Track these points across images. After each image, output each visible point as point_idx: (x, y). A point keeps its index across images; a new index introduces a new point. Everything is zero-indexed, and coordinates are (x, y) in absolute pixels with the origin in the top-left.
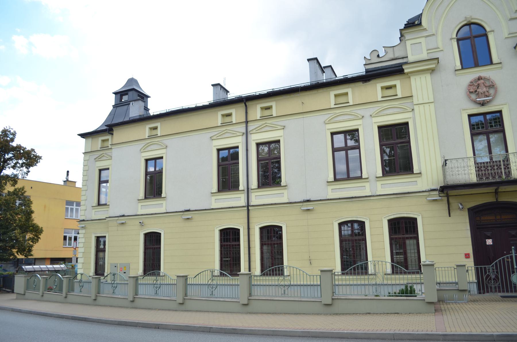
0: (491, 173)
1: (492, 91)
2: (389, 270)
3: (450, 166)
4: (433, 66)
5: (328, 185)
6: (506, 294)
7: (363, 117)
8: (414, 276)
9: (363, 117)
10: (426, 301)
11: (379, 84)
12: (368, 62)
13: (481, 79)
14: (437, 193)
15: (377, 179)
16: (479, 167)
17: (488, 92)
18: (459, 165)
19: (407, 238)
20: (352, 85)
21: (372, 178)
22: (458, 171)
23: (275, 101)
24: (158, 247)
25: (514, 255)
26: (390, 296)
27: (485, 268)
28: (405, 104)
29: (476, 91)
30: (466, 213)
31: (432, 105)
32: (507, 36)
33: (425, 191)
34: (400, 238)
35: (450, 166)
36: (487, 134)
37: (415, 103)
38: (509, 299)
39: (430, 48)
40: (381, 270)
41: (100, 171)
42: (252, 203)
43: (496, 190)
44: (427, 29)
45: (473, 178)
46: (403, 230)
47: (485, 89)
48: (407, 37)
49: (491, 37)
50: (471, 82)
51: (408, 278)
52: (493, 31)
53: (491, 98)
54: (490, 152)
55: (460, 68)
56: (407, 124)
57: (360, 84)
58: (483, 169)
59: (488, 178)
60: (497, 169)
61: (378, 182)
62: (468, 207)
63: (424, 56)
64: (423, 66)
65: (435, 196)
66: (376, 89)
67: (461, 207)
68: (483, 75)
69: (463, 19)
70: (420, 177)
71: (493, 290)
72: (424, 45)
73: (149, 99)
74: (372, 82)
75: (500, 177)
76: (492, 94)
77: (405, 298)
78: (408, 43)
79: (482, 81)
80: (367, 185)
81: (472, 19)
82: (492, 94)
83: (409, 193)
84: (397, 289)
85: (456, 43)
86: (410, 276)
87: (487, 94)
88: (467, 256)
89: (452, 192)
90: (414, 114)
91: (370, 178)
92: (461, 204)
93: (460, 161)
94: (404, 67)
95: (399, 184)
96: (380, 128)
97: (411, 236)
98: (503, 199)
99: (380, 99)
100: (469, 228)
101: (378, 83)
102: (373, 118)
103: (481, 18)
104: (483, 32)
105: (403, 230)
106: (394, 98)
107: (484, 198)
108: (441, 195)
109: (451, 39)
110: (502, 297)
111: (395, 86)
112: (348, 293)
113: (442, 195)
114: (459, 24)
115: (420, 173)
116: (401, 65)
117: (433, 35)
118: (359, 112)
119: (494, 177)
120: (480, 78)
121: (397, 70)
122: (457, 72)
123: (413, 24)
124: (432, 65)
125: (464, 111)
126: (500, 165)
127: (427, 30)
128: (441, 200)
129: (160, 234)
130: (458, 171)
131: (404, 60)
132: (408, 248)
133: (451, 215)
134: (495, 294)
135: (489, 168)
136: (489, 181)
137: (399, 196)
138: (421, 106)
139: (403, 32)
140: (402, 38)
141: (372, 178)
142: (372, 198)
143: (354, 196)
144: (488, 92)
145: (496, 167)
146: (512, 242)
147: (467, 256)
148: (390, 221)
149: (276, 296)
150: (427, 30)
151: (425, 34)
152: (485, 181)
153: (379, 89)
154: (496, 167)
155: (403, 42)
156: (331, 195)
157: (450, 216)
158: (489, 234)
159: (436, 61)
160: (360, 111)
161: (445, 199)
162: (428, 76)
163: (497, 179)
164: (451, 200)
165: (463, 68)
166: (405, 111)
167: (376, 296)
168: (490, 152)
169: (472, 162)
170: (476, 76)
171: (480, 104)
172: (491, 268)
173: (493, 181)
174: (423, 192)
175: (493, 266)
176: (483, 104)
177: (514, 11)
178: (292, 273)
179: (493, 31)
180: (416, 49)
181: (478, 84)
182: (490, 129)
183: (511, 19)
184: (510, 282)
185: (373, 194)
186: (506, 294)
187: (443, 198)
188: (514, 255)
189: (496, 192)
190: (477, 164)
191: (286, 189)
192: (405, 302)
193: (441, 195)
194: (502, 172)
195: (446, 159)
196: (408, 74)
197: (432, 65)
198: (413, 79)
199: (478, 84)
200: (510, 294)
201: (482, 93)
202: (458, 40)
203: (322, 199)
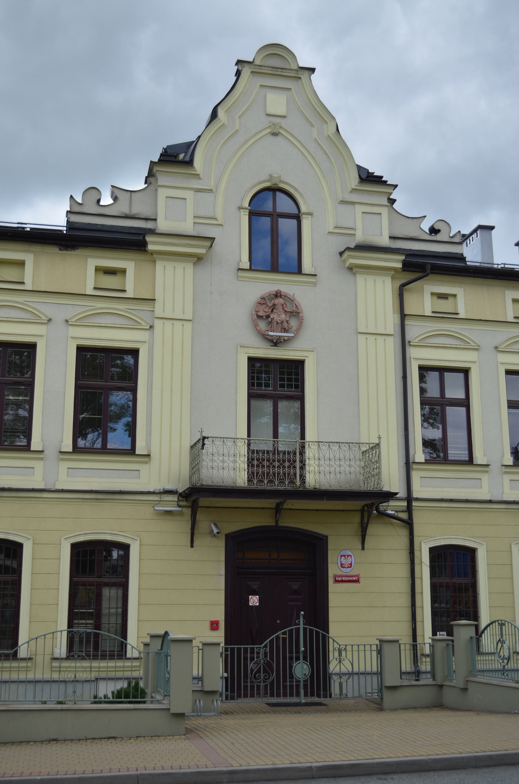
0: (279, 474)
1: (294, 323)
2: (62, 650)
3: (210, 451)
4: (202, 251)
5: (62, 460)
6: (275, 700)
7: (50, 320)
8: (111, 664)
9: (50, 320)
10: (173, 711)
11: (94, 260)
12: (77, 209)
13: (281, 296)
14: (175, 498)
15: (61, 457)
16: (255, 459)
17: (287, 322)
18: (226, 451)
19: (107, 585)
20: (37, 248)
21: (51, 452)
22: (223, 461)
23: (32, 252)
24: (75, 579)
25: (301, 626)
26: (95, 703)
27: (239, 650)
28: (140, 312)
29: (268, 317)
30: (221, 544)
31: (188, 326)
32: (331, 230)
33: (153, 493)
34: (91, 584)
35: (210, 451)
36: (276, 399)
37: (158, 312)
38: (284, 708)
39: (201, 213)
40: (48, 650)
41: (466, 372)
42: (415, 495)
43: (278, 505)
44: (201, 176)
45: (240, 477)
46: (98, 567)
47: (283, 317)
48: (162, 180)
49: (306, 223)
50: (263, 298)
51: (76, 667)
52: (311, 214)
53: (292, 335)
54: (276, 435)
55: (247, 266)
56: (32, 347)
57: (55, 250)
58: (265, 463)
59: (270, 481)
60: (289, 467)
61: (61, 463)
62: (227, 532)
63: (187, 226)
64: (386, 260)
65: (170, 503)
66: (84, 269)
67: (215, 531)
68: (284, 289)
69: (266, 177)
70: (146, 463)
71: (262, 691)
72: (190, 203)
73: (493, 231)
74: (80, 252)
75: (292, 482)
76: (294, 328)
77: (131, 706)
78: (162, 193)
79: (279, 301)
80: (39, 466)
81: (281, 182)
82: (294, 328)
83: (121, 493)
84: (106, 689)
85: (247, 217)
86: (103, 664)
87: (285, 325)
88: (214, 626)
89: (204, 501)
90: (152, 336)
91: (46, 452)
92: (216, 525)
93: (335, 447)
94: (148, 239)
95: (99, 473)
96: (81, 350)
97: (114, 580)
98: (288, 522)
99: (90, 291)
100: (223, 572)
101: (91, 257)
102: (71, 329)
103: (295, 185)
104: (293, 210)
105: (98, 567)
106: (118, 295)
107: (254, 518)
108: (181, 503)
109: (240, 208)
110: (269, 704)
111: (123, 272)
112: (30, 697)
113: (184, 503)
114: (260, 183)
115: (149, 455)
116: (144, 232)
117: (211, 191)
118: (43, 308)
119: (282, 482)
120: (278, 295)
121: (132, 240)
122: (241, 274)
123: (176, 158)
124: (198, 249)
125: (243, 350)
126: (295, 461)
127: (200, 178)
128: (181, 514)
129: (471, 552)
130: (223, 461)
131: (149, 225)
132: (105, 604)
133: (195, 544)
134: (239, 700)
135: (276, 464)
136: (273, 488)
137: (100, 496)
138: (168, 323)
139: (156, 168)
140: (151, 179)
141: (51, 452)
142: (45, 495)
143: (6, 486)
144: (287, 322)
145: (287, 464)
146: (290, 603)
147: (214, 626)
148: (74, 546)
149: (25, 702)
150: (200, 178)
151: (195, 184)
152: (266, 486)
153: (91, 271)
154: (287, 464)
155: (152, 187)
156: (65, 482)
157: (192, 546)
158: (255, 585)
159: (208, 244)
160: (46, 307)
161: (188, 512)
162: (189, 268)
163: (286, 486)
164: (199, 517)
165: (251, 269)
166: (135, 327)
167: (61, 703)
168: (276, 435)
169: (243, 450)
170: (273, 288)
171: (271, 341)
172: (262, 651)
173: (269, 488)
174: (149, 493)
175: (266, 646)
176: (276, 343)
177: (350, 189)
178: (40, 651)
179: (311, 214)
180: (175, 210)
181: (274, 305)
182: (281, 391)
183: (342, 202)
184: (292, 676)
185: (48, 487)
186: (275, 700)
187: (185, 510)
188: (301, 626)
189: (278, 509)
190: (253, 451)
191: (487, 472)
192: (128, 715)
193: (181, 503)
194: (295, 474)
195: (204, 434)
196: (152, 253)
197: (198, 249)
198: (160, 265)
199: (274, 305)
200: (282, 700)
201: (277, 323)
202: (252, 214)
203: (469, 498)
